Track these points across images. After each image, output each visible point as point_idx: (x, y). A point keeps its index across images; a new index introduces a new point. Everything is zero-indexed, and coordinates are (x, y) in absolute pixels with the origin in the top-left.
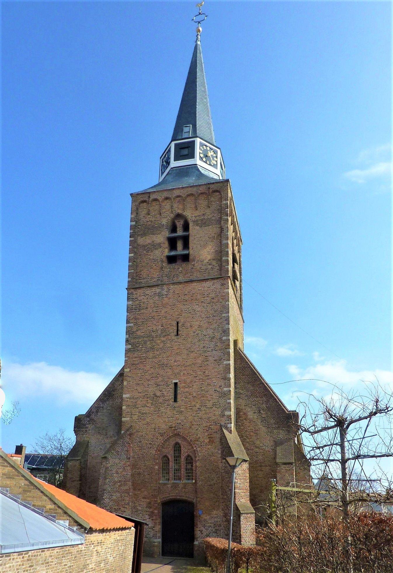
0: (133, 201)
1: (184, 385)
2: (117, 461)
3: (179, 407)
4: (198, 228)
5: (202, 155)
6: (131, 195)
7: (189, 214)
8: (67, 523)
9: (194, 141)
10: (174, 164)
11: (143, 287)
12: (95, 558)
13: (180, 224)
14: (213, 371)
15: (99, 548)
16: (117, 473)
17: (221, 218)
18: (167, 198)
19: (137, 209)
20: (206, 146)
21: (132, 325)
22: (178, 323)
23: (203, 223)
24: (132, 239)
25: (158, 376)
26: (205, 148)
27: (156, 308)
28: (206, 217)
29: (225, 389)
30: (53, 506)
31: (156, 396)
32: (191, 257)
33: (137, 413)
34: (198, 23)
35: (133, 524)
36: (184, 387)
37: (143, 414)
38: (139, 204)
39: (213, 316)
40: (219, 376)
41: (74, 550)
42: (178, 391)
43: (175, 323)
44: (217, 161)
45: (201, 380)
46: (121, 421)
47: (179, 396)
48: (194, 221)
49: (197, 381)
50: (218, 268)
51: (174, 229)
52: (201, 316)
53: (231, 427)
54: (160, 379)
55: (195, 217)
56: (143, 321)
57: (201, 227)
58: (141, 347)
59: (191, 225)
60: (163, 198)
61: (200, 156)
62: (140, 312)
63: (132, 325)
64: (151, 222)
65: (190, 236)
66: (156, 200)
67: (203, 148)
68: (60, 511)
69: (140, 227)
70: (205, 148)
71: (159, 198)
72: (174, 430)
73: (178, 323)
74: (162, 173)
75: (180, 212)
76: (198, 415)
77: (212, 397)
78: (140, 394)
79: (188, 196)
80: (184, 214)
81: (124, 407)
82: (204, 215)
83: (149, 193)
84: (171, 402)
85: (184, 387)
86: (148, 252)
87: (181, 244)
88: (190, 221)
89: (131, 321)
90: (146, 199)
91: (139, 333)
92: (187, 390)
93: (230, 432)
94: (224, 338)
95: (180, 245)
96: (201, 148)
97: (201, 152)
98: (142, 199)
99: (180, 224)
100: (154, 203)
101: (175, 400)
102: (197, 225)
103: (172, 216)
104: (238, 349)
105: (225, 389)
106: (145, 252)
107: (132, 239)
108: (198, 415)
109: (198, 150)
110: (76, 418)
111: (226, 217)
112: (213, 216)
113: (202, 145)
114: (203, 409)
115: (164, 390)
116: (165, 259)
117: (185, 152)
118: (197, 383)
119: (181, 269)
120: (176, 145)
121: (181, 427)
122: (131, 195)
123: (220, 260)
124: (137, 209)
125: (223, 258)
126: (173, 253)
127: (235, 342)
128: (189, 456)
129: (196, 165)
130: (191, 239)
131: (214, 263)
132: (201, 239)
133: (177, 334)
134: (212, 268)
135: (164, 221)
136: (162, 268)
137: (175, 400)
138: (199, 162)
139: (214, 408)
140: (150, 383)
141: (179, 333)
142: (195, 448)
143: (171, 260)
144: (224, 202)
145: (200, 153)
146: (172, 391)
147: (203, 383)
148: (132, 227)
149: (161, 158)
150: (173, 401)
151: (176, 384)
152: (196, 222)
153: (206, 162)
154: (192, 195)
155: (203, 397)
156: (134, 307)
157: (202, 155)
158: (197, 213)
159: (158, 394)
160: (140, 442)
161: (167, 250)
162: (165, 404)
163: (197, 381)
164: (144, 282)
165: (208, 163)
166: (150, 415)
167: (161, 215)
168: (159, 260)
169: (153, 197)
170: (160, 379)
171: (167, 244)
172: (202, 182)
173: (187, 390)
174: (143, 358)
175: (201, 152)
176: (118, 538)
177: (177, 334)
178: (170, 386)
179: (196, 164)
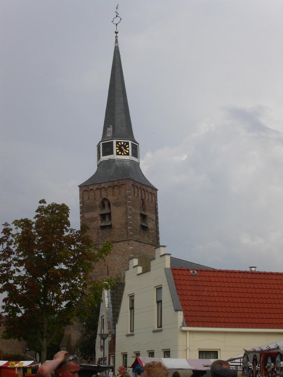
0: (80, 190)
4: (115, 207)
5: (118, 151)
6: (79, 186)
7: (110, 198)
9: (113, 142)
13: (106, 203)
18: (98, 189)
19: (83, 196)
20: (121, 142)
22: (108, 267)
26: (120, 144)
28: (119, 201)
32: (113, 226)
39: (125, 263)
43: (106, 267)
50: (126, 233)
51: (103, 206)
52: (119, 263)
55: (113, 200)
57: (116, 207)
59: (111, 205)
60: (96, 188)
64: (91, 203)
65: (111, 213)
66: (92, 189)
69: (85, 206)
70: (120, 144)
73: (108, 267)
80: (107, 198)
82: (118, 199)
88: (111, 203)
90: (87, 189)
95: (107, 219)
96: (117, 145)
100: (92, 191)
102: (115, 206)
103: (101, 200)
106: (89, 223)
107: (81, 215)
109: (115, 148)
112: (123, 200)
113: (117, 143)
116: (99, 227)
119: (108, 234)
122: (79, 186)
124: (83, 196)
125: (129, 228)
126: (103, 224)
130: (112, 214)
131: (124, 230)
133: (108, 274)
134: (123, 233)
136: (98, 233)
141: (109, 273)
143: (103, 228)
145: (117, 150)
149: (97, 146)
153: (121, 155)
154: (110, 186)
157: (118, 151)
158: (115, 198)
161: (100, 222)
165: (119, 143)
167: (95, 199)
168: (96, 228)
171: (99, 218)
175: (118, 148)
177: (108, 274)
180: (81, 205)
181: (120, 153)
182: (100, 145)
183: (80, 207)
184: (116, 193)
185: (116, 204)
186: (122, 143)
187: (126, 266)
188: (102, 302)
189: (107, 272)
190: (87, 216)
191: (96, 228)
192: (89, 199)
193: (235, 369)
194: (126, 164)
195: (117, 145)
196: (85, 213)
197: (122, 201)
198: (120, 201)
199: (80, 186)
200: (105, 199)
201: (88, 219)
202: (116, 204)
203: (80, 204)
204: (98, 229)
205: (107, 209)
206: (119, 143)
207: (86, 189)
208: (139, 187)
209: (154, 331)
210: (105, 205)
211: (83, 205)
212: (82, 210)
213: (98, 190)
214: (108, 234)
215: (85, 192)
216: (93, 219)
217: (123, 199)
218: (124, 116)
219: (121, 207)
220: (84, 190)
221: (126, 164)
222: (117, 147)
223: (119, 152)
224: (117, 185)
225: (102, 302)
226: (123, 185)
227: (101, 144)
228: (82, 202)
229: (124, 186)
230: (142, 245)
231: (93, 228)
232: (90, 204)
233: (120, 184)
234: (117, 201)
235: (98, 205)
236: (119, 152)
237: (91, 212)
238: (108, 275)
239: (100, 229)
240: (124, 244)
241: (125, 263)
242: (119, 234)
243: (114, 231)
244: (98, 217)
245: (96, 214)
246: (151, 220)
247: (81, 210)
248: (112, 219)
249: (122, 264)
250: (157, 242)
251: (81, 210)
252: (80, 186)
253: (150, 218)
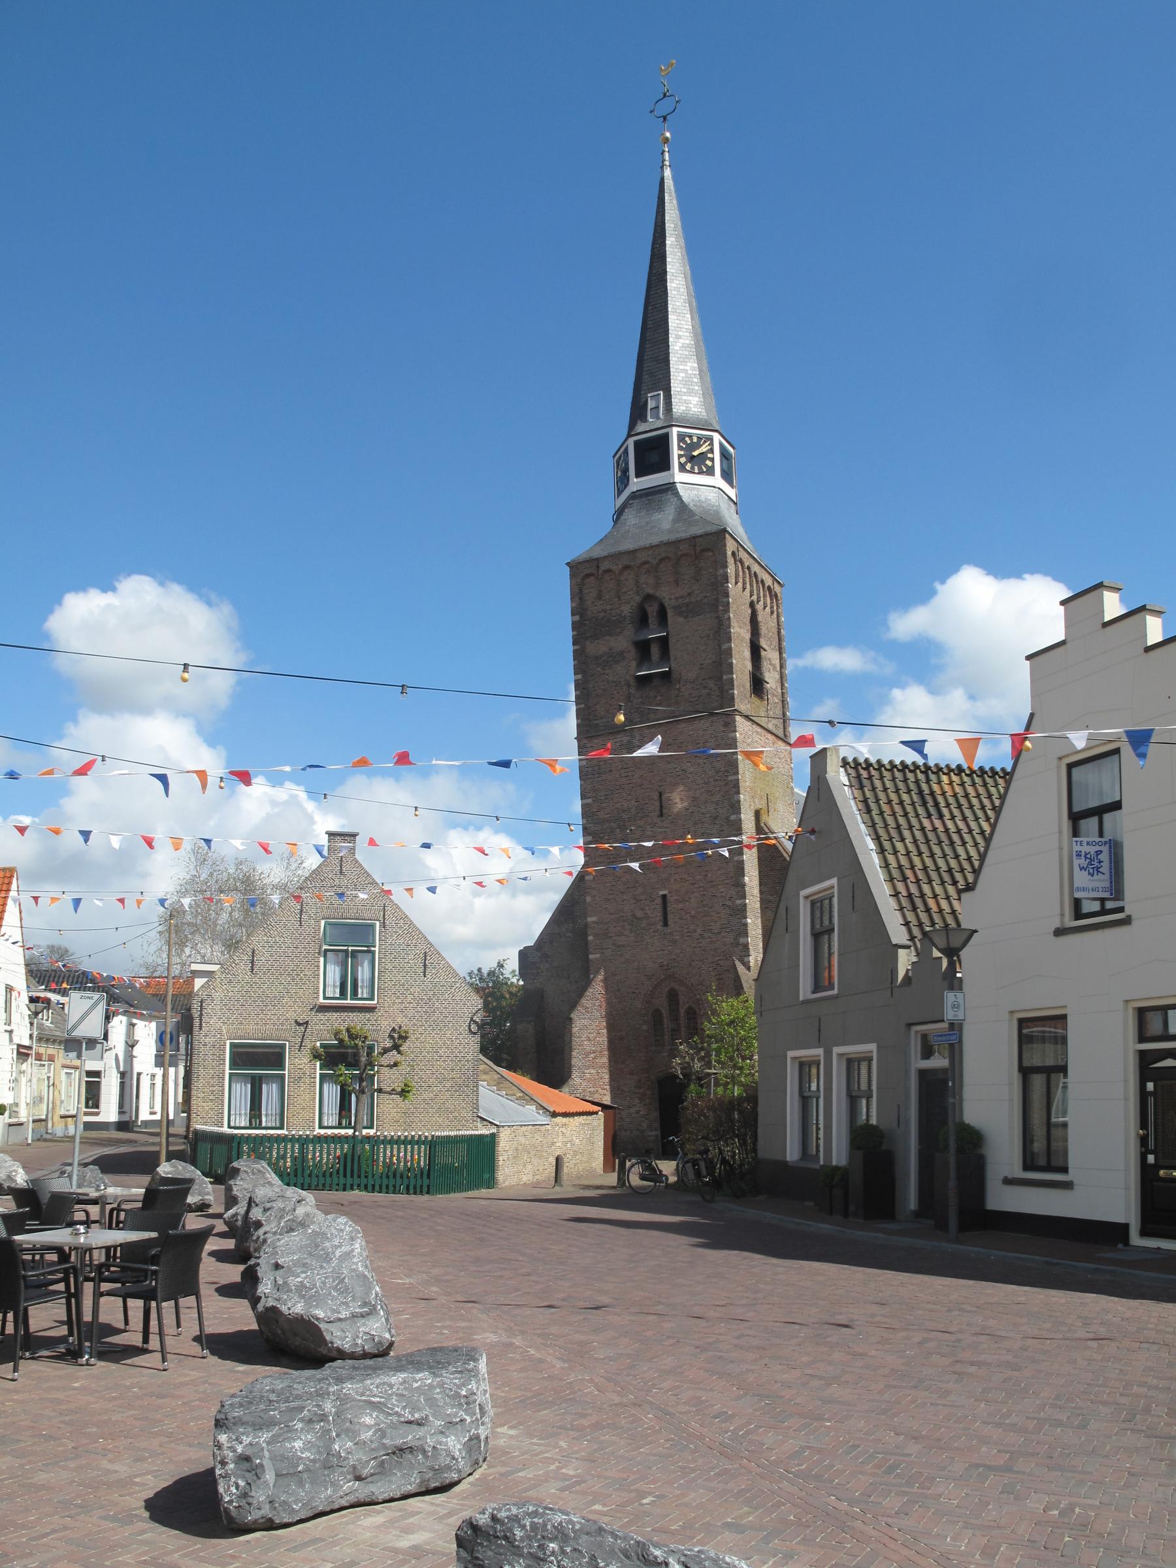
0: (572, 576)
1: (677, 898)
2: (585, 1022)
3: (671, 934)
4: (681, 619)
6: (568, 564)
7: (667, 594)
8: (534, 1108)
10: (637, 483)
11: (602, 735)
12: (560, 1138)
13: (652, 610)
14: (719, 872)
15: (564, 1130)
16: (589, 1040)
17: (717, 600)
18: (626, 567)
19: (581, 591)
20: (690, 437)
21: (589, 801)
23: (689, 610)
24: (576, 647)
25: (637, 885)
27: (626, 770)
28: (693, 600)
29: (738, 902)
30: (521, 1094)
31: (636, 918)
32: (675, 675)
33: (611, 946)
34: (662, 119)
35: (600, 1108)
36: (678, 901)
37: (619, 946)
38: (583, 579)
39: (715, 780)
40: (726, 882)
41: (542, 1128)
42: (669, 909)
43: (656, 796)
44: (712, 460)
45: (701, 889)
46: (587, 960)
47: (670, 917)
48: (675, 608)
49: (695, 890)
50: (717, 693)
51: (642, 620)
53: (749, 962)
54: (640, 890)
55: (677, 599)
56: (607, 793)
57: (686, 618)
58: (606, 837)
59: (670, 614)
60: (621, 566)
61: (680, 463)
62: (600, 779)
63: (589, 801)
64: (605, 611)
66: (609, 571)
67: (685, 442)
68: (527, 1097)
69: (587, 622)
70: (689, 442)
71: (614, 568)
72: (667, 970)
74: (620, 492)
75: (651, 591)
76: (701, 945)
77: (719, 915)
78: (612, 916)
79: (661, 560)
80: (658, 594)
81: (590, 938)
82: (689, 594)
83: (597, 560)
84: (659, 927)
85: (678, 901)
86: (603, 669)
87: (657, 649)
89: (589, 795)
91: (601, 815)
92: (681, 906)
93: (749, 968)
94: (733, 817)
95: (655, 651)
96: (681, 444)
97: (682, 453)
98: (587, 571)
99: (652, 610)
101: (666, 924)
102: (680, 614)
103: (638, 599)
104: (762, 825)
105: (738, 902)
106: (599, 669)
107: (576, 647)
108: (701, 945)
110: (521, 952)
111: (725, 600)
113: (681, 438)
114: (706, 935)
115: (646, 908)
116: (632, 682)
117: (654, 457)
118: (696, 894)
120: (637, 444)
121: (676, 964)
122: (568, 564)
123: (720, 678)
125: (725, 677)
127: (757, 814)
128: (690, 1008)
129: (671, 485)
130: (672, 642)
131: (711, 684)
132: (688, 641)
133: (661, 815)
135: (626, 610)
137: (666, 924)
138: (679, 477)
139: (723, 934)
140: (625, 897)
141: (664, 811)
142: (698, 997)
144: (721, 571)
145: (680, 456)
146: (659, 908)
147: (705, 893)
148: (575, 626)
149: (614, 457)
150: (662, 924)
151: (664, 896)
152: (679, 611)
155: (706, 916)
156: (590, 769)
157: (683, 460)
159: (639, 914)
160: (619, 990)
161: (634, 664)
162: (652, 930)
163: (695, 890)
164: (601, 724)
165: (687, 439)
166: (630, 948)
169: (605, 566)
170: (640, 890)
171: (632, 653)
172: (684, 532)
173: (681, 906)
174: (611, 857)
175: (682, 453)
176: (583, 1122)
177: (661, 815)
178: (656, 901)
179: (675, 483)
180: (577, 618)
181: (688, 467)
182: (626, 452)
183: (573, 623)
184: (686, 577)
185: (684, 609)
186: (695, 440)
187: (718, 789)
188: (768, 683)
189: (658, 808)
190: (592, 648)
191: (623, 683)
192: (599, 597)
193: (856, 1088)
194: (706, 499)
195: (681, 444)
196: (588, 643)
197: (704, 601)
198: (699, 599)
199: (575, 567)
200: (648, 598)
201: (597, 658)
202: (684, 609)
203: (575, 674)
204: (629, 686)
205: (655, 627)
206: (687, 439)
207: (590, 571)
208: (746, 564)
209: (1059, 932)
210: (650, 616)
211: (581, 616)
212: (578, 632)
213: (626, 573)
214: (659, 698)
215: (587, 581)
216: (615, 657)
217: (708, 595)
218: (696, 365)
219: (702, 617)
220: (582, 575)
221: (706, 499)
222: (680, 448)
223: (686, 463)
224: (686, 555)
225: (768, 683)
226: (705, 553)
227: (631, 443)
228: (579, 610)
229: (710, 554)
230: (757, 733)
231: (614, 682)
232: (602, 614)
233: (698, 549)
234: (688, 600)
235: (630, 614)
236: (686, 463)
237: (607, 638)
238: (662, 819)
239: (633, 684)
240: (711, 726)
241: (715, 780)
242: (693, 696)
243: (679, 689)
244: (629, 652)
245: (623, 641)
246: (771, 668)
247: (575, 633)
248: (672, 652)
249: (706, 783)
250: (784, 731)
251: (575, 633)
252: (575, 567)
253: (770, 659)
